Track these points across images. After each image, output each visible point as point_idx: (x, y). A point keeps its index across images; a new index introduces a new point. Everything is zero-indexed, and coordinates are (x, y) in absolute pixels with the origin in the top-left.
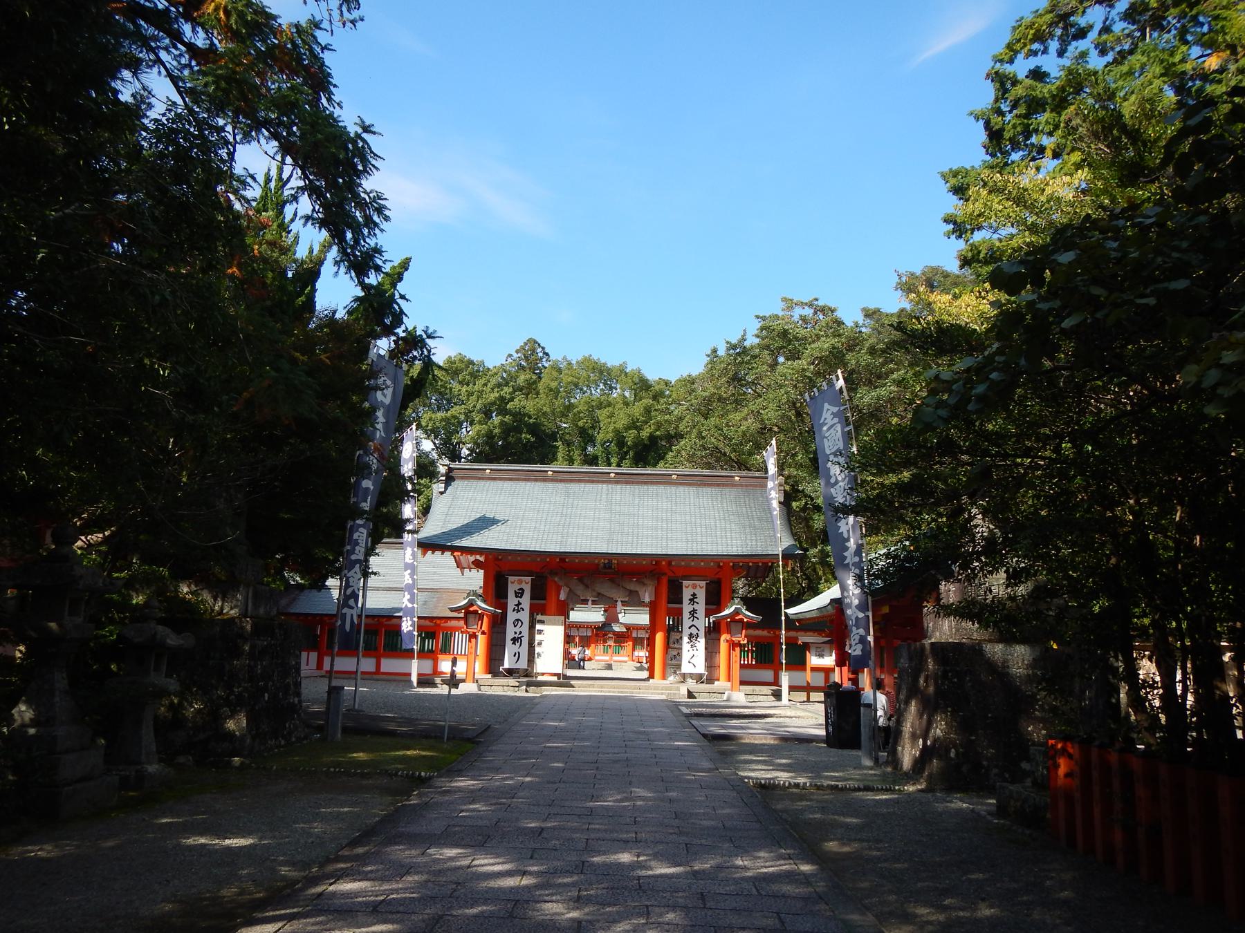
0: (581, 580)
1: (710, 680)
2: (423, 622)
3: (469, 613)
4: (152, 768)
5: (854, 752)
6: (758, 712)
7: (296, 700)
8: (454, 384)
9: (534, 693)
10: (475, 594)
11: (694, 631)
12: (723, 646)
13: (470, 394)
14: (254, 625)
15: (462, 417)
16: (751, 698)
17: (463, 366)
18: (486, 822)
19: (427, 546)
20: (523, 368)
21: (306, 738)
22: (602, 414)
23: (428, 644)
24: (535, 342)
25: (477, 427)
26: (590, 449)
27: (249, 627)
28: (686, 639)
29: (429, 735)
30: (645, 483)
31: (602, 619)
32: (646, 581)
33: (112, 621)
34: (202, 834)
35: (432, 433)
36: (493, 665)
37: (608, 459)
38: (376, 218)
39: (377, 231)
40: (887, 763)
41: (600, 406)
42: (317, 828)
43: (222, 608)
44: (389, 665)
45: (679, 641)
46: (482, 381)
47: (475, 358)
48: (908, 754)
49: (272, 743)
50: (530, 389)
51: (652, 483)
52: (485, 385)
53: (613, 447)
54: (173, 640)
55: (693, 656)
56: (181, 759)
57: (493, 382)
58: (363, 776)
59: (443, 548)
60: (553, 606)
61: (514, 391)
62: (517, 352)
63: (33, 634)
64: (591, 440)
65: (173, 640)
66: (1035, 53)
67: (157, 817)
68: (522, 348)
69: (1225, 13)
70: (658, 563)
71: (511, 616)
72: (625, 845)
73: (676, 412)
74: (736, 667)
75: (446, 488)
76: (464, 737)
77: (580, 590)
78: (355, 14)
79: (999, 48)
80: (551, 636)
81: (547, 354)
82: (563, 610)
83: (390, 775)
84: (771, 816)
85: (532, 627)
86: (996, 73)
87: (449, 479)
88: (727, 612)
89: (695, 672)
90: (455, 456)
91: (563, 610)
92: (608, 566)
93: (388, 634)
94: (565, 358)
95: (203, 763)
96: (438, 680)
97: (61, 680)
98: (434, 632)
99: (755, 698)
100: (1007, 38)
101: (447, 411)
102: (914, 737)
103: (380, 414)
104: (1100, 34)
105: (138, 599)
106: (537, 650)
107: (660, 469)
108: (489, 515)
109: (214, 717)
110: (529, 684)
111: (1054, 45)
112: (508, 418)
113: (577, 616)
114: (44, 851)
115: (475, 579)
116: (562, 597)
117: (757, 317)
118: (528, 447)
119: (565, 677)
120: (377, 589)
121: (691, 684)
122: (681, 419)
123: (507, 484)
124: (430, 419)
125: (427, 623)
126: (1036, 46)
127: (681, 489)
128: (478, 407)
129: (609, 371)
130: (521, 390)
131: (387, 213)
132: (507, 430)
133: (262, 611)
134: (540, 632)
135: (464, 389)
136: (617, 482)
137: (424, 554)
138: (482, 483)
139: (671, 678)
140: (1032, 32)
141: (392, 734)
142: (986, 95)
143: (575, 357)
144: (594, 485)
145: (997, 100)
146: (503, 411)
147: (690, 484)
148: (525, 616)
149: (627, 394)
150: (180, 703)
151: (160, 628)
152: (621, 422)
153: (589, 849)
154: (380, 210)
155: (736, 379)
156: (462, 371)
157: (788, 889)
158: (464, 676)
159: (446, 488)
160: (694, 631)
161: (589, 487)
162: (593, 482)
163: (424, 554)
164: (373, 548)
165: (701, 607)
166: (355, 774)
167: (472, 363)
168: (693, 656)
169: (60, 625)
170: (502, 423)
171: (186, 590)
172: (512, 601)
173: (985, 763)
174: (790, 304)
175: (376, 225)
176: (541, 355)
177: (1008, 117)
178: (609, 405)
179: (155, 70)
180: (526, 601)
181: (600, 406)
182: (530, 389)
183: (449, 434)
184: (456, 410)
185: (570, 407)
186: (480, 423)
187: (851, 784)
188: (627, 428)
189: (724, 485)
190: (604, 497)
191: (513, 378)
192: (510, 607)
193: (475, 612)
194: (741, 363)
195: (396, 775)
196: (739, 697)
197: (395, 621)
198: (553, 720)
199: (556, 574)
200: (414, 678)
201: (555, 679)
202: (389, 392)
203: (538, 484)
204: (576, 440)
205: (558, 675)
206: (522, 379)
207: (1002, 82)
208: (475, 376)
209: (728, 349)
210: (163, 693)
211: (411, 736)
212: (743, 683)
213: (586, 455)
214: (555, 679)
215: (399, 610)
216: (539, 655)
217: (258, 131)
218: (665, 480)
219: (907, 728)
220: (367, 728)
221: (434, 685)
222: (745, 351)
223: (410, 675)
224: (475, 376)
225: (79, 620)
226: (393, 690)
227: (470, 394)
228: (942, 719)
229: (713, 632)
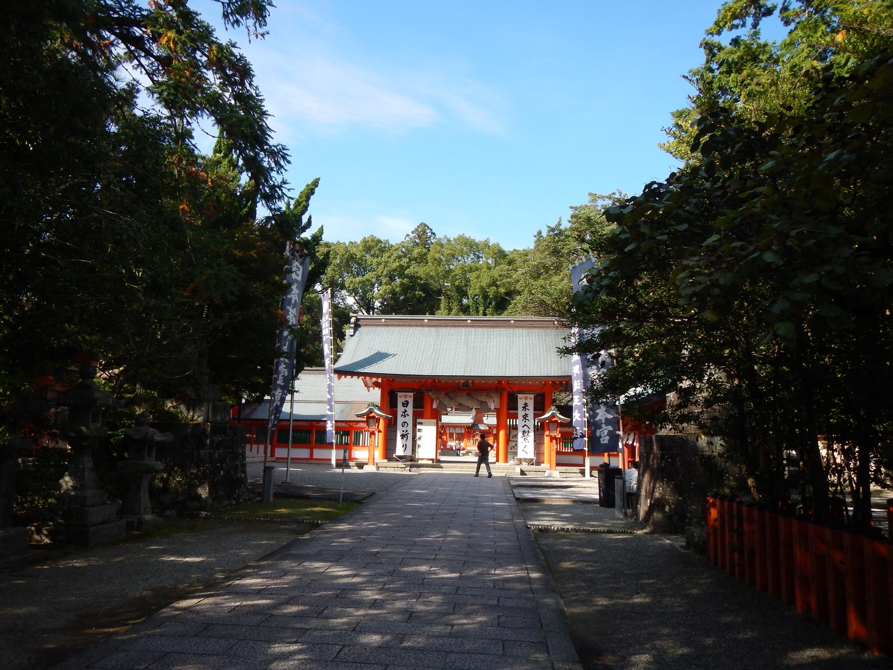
0: (447, 395)
1: (538, 463)
2: (340, 424)
3: (369, 418)
4: (148, 517)
5: (611, 509)
6: (539, 483)
7: (243, 475)
8: (368, 256)
9: (415, 472)
10: (373, 405)
11: (526, 429)
12: (547, 440)
13: (379, 264)
14: (212, 428)
15: (374, 280)
16: (564, 475)
17: (374, 244)
18: (345, 548)
19: (340, 372)
20: (417, 244)
21: (249, 500)
22: (472, 276)
23: (345, 439)
24: (426, 225)
25: (384, 287)
26: (465, 301)
27: (209, 429)
28: (520, 434)
29: (331, 498)
30: (492, 327)
31: (472, 421)
32: (491, 394)
33: (124, 426)
34: (172, 555)
35: (354, 292)
36: (388, 452)
37: (477, 308)
38: (282, 162)
39: (283, 170)
40: (632, 516)
41: (471, 270)
42: (245, 553)
43: (193, 417)
44: (318, 453)
45: (516, 436)
46: (387, 255)
47: (382, 238)
48: (643, 507)
49: (226, 502)
50: (422, 259)
51: (497, 327)
52: (389, 257)
53: (481, 300)
54: (158, 437)
55: (526, 446)
56: (168, 512)
57: (395, 255)
58: (281, 523)
59: (352, 374)
60: (428, 411)
61: (410, 261)
62: (413, 232)
63: (73, 435)
64: (464, 294)
65: (158, 437)
66: (737, 27)
67: (148, 546)
68: (417, 230)
69: (841, 6)
70: (500, 382)
71: (400, 420)
72: (426, 561)
73: (514, 276)
74: (554, 453)
75: (355, 332)
76: (354, 499)
77: (446, 401)
78: (264, 29)
79: (710, 25)
80: (428, 433)
81: (434, 234)
82: (436, 416)
83: (299, 522)
84: (538, 548)
85: (414, 426)
86: (706, 43)
87: (357, 326)
88: (546, 416)
89: (524, 458)
90: (369, 308)
91: (436, 416)
92: (466, 384)
93: (318, 432)
94: (445, 237)
95: (181, 515)
96: (351, 464)
97: (88, 462)
98: (349, 432)
99: (568, 475)
100: (715, 17)
101: (363, 276)
102: (646, 498)
103: (294, 287)
104: (781, 12)
105: (139, 411)
106: (418, 442)
107: (503, 317)
108: (383, 351)
109: (191, 487)
110: (412, 466)
111: (750, 20)
112: (405, 281)
113: (445, 419)
114: (78, 563)
115: (375, 395)
116: (434, 406)
117: (571, 207)
118: (420, 300)
119: (439, 461)
120: (299, 402)
121: (525, 466)
122: (518, 281)
123: (397, 329)
124: (351, 282)
125: (344, 425)
126: (736, 22)
127: (517, 330)
128: (385, 273)
129: (477, 245)
130: (415, 259)
131: (288, 158)
132: (405, 289)
133: (219, 418)
134: (420, 430)
135: (375, 261)
136: (472, 326)
137: (339, 378)
138: (379, 328)
139: (511, 462)
140: (730, 14)
141: (308, 498)
142: (699, 58)
143: (453, 235)
144: (457, 329)
145: (707, 62)
146: (402, 275)
147: (523, 327)
148: (409, 419)
149: (490, 261)
150: (168, 478)
151: (151, 429)
152: (485, 281)
153: (402, 563)
154: (284, 158)
155: (556, 252)
156: (373, 247)
157: (518, 586)
158: (366, 461)
159: (355, 332)
160: (526, 429)
161: (453, 330)
162: (455, 326)
163: (339, 378)
164: (296, 376)
165: (531, 412)
166: (277, 522)
167: (380, 242)
168: (526, 446)
169: (88, 428)
170: (402, 284)
171: (169, 405)
172: (400, 409)
173: (689, 515)
174: (594, 197)
175: (282, 167)
176: (429, 234)
177: (717, 73)
178: (477, 269)
179: (139, 70)
180: (410, 409)
181: (471, 270)
182: (422, 259)
183: (365, 292)
184: (369, 275)
185: (450, 271)
186: (386, 284)
187: (602, 529)
188: (490, 286)
189: (547, 327)
190: (463, 338)
191: (409, 251)
192: (400, 413)
193: (374, 417)
194: (558, 241)
195: (302, 522)
196: (556, 474)
197: (321, 424)
198: (419, 489)
199: (430, 391)
200: (333, 462)
201: (430, 462)
202: (300, 273)
203: (418, 328)
204: (454, 294)
205: (433, 460)
206: (416, 252)
207: (711, 49)
208: (382, 250)
209: (549, 232)
210: (152, 470)
211: (320, 499)
212: (558, 465)
213: (462, 305)
214: (430, 462)
215: (325, 416)
216: (419, 446)
217: (202, 111)
218: (505, 324)
219: (643, 493)
220: (291, 494)
221: (348, 467)
222: (561, 233)
223: (330, 460)
224: (382, 250)
225: (99, 425)
226: (319, 471)
227: (379, 264)
228: (660, 486)
229: (539, 430)
